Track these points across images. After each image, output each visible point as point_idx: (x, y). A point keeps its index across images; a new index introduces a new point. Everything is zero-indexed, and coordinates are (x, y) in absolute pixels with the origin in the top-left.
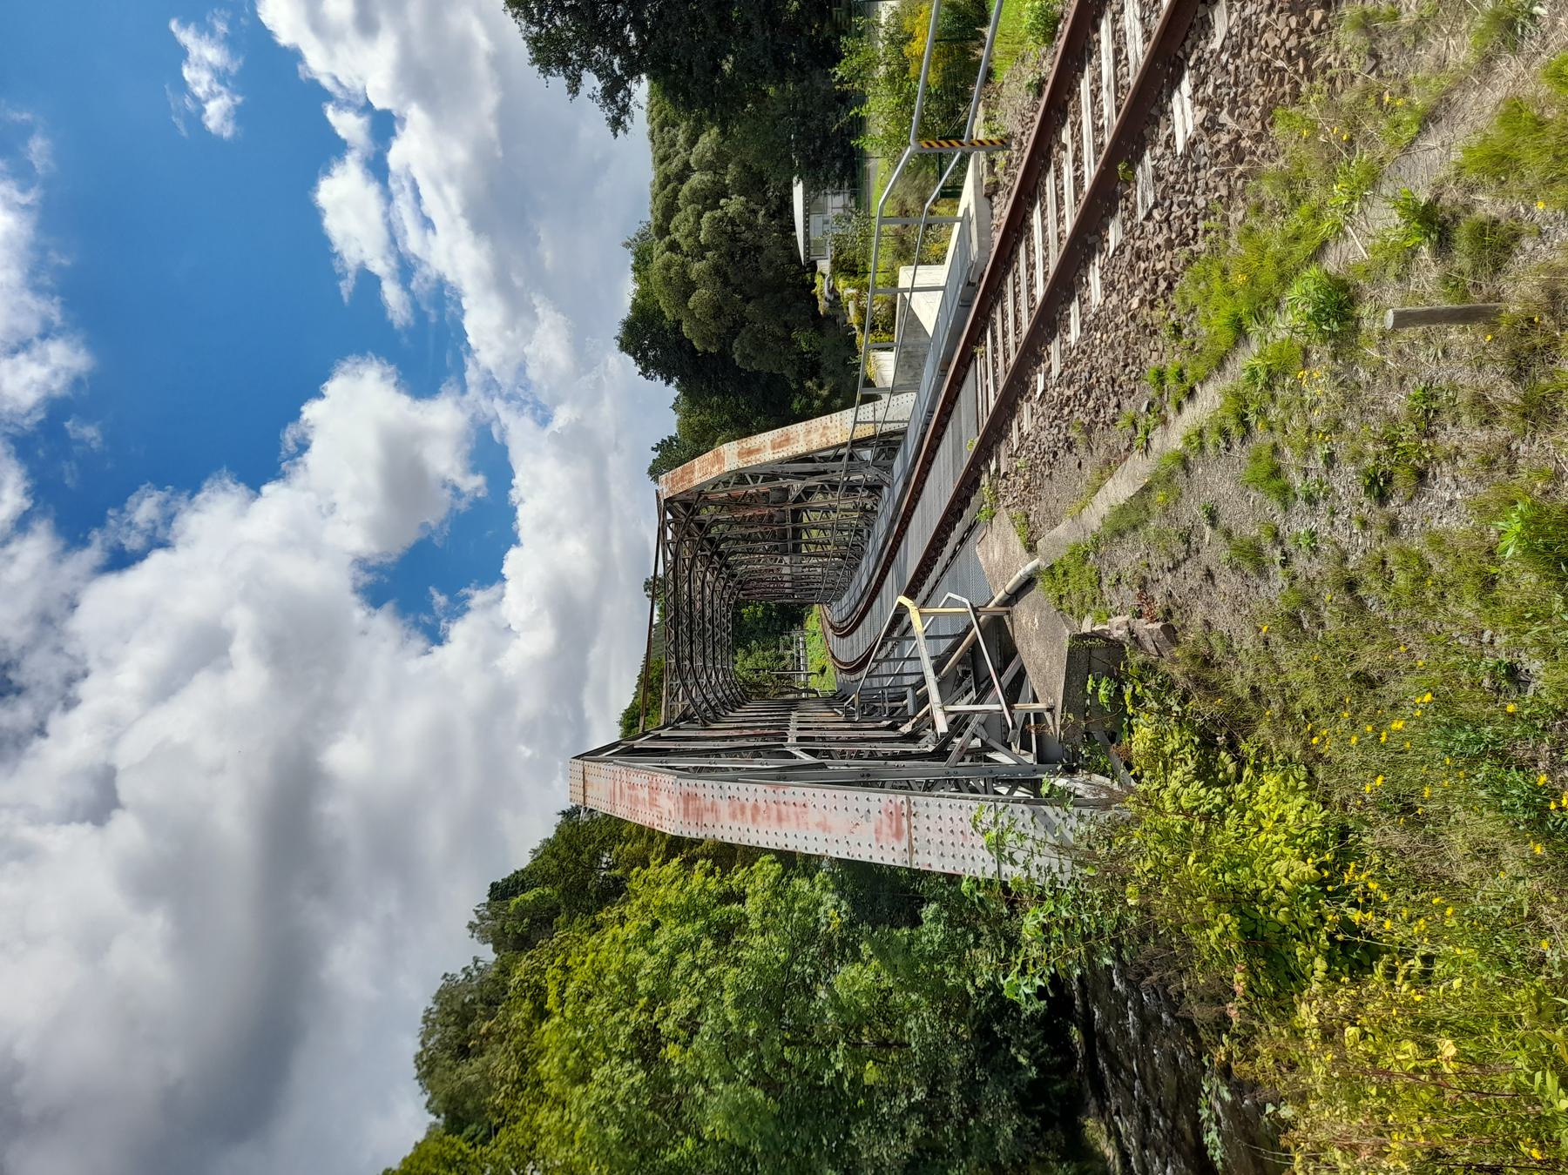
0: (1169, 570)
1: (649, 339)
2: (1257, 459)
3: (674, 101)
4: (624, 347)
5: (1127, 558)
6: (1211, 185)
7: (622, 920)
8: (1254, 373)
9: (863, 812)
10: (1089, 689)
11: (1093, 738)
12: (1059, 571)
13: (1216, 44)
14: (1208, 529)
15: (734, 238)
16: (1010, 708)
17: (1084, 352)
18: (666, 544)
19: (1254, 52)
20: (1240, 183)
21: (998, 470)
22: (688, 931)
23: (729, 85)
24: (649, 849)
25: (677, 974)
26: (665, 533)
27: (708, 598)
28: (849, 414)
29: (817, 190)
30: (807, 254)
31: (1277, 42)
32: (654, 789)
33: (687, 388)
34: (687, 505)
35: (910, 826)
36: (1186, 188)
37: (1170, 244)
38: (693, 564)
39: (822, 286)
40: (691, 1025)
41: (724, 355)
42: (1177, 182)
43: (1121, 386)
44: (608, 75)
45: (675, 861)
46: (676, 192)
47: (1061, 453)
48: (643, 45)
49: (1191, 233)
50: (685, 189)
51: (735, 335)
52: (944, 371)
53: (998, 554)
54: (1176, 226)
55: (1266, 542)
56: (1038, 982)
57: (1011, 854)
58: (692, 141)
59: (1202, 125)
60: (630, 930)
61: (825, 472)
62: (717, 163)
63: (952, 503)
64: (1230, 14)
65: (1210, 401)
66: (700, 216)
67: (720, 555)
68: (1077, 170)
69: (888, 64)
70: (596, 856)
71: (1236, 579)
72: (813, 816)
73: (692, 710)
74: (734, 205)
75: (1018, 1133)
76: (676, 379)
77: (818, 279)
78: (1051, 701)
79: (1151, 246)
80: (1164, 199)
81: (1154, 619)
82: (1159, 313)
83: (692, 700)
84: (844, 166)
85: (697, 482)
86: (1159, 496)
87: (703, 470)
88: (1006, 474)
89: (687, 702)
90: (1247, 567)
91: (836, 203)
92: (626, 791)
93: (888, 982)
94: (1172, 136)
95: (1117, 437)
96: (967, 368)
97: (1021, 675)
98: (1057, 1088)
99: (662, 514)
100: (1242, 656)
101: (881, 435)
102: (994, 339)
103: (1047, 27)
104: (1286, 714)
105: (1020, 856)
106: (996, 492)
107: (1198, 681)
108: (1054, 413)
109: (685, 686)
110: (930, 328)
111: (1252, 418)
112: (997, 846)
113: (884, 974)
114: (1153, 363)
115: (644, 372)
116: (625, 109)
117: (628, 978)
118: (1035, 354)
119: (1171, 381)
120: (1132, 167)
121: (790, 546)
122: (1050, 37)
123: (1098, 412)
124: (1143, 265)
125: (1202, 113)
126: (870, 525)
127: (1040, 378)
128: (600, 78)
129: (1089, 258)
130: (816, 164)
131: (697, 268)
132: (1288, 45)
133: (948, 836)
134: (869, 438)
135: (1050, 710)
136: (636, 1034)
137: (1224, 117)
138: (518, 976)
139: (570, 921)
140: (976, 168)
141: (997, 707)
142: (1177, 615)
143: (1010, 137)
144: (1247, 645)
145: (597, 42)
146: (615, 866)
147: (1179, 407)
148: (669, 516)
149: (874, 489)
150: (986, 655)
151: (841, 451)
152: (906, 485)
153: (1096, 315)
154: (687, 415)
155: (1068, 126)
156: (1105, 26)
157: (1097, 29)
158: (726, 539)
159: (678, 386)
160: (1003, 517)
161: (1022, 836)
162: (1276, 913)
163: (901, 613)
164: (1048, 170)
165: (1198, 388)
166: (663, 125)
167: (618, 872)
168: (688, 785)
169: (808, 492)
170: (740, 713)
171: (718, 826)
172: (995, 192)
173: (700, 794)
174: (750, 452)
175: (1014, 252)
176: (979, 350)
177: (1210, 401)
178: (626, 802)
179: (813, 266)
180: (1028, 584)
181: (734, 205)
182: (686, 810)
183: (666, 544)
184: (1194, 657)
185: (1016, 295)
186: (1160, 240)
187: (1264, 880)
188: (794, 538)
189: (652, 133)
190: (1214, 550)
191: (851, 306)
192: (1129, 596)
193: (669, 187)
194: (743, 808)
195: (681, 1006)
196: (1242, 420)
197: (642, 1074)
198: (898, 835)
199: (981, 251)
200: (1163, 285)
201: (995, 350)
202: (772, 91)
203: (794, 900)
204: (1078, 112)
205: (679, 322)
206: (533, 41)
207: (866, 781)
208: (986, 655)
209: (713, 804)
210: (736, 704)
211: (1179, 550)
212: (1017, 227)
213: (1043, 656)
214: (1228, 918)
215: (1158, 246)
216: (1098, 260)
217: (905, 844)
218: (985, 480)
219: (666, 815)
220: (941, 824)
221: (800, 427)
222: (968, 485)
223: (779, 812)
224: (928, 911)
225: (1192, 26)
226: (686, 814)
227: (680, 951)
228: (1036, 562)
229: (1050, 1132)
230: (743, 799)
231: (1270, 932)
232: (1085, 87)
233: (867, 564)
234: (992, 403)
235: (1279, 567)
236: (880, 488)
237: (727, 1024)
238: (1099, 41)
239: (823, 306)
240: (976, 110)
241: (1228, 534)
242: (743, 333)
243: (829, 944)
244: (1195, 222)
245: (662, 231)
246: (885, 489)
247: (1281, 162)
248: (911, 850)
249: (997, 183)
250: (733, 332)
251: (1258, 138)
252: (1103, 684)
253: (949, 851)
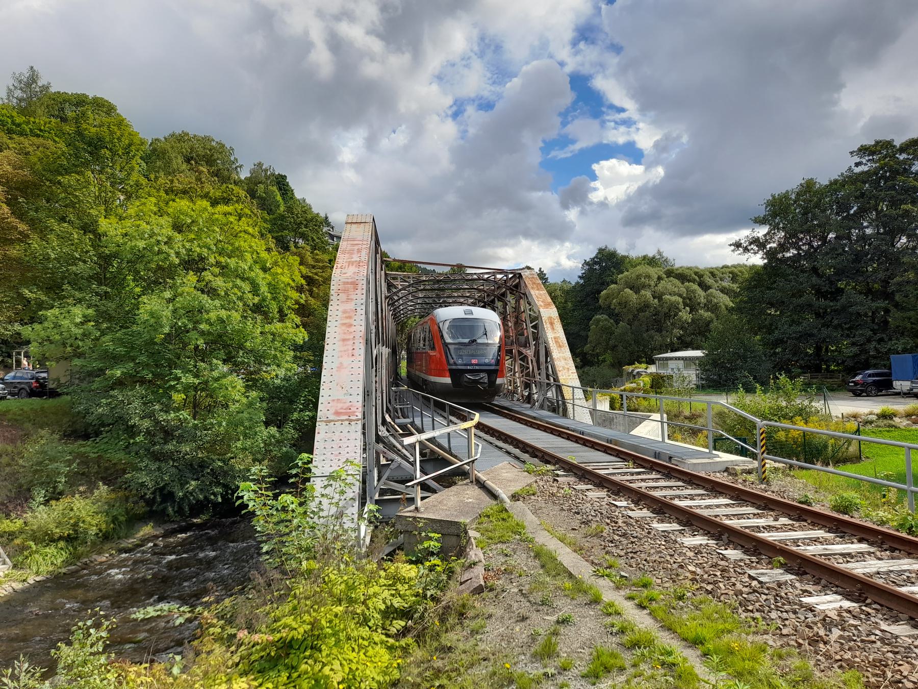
0: (521, 591)
2: (613, 655)
4: (601, 251)
5: (521, 560)
6: (787, 623)
7: (268, 250)
8: (670, 653)
9: (351, 391)
10: (432, 535)
11: (397, 537)
14: (554, 618)
17: (649, 533)
18: (494, 274)
19: (890, 655)
20: (793, 643)
21: (558, 475)
22: (264, 289)
23: (762, 312)
25: (238, 282)
26: (500, 273)
27: (458, 300)
28: (577, 383)
30: (660, 359)
31: (905, 673)
32: (358, 264)
33: (577, 289)
34: (517, 286)
35: (342, 421)
36: (779, 604)
37: (738, 593)
38: (480, 291)
39: (640, 368)
40: (211, 292)
41: (598, 309)
42: (782, 597)
43: (632, 558)
44: (767, 240)
45: (303, 282)
46: (694, 281)
47: (579, 517)
48: (784, 260)
49: (750, 608)
50: (695, 287)
51: (609, 315)
52: (610, 441)
53: (506, 475)
54: (752, 597)
56: (251, 504)
57: (331, 485)
58: (723, 290)
59: (826, 616)
61: (539, 369)
62: (712, 307)
63: (523, 443)
64: (909, 637)
65: (642, 621)
66: (680, 296)
68: (763, 527)
70: (303, 236)
71: (524, 637)
72: (346, 361)
73: (394, 290)
74: (685, 315)
75: (142, 485)
76: (582, 281)
77: (644, 365)
78: (422, 509)
79: (733, 580)
80: (768, 589)
81: (485, 578)
83: (400, 290)
84: (714, 381)
85: (532, 292)
86: (568, 584)
88: (557, 481)
89: (400, 287)
90: (536, 648)
91: (692, 375)
92: (356, 248)
93: (233, 408)
94: (810, 594)
96: (617, 456)
97: (434, 491)
98: (170, 509)
99: (512, 272)
100: (472, 641)
101: (564, 404)
102: (639, 473)
103: (845, 508)
104: (438, 673)
105: (328, 491)
106: (543, 474)
107: (447, 608)
108: (604, 512)
109: (409, 286)
110: (634, 432)
111: (638, 652)
113: (237, 405)
115: (586, 263)
116: (746, 250)
117: (237, 253)
118: (639, 500)
119: (645, 592)
120: (782, 566)
122: (837, 508)
123: (612, 542)
124: (718, 573)
125: (833, 615)
127: (624, 504)
128: (765, 236)
129: (712, 536)
132: (905, 681)
133: (338, 448)
135: (416, 508)
136: (202, 259)
137: (836, 632)
138: (236, 189)
139: (265, 221)
140: (744, 462)
141: (418, 476)
142: (491, 595)
143: (768, 483)
144: (482, 646)
145: (786, 233)
146: (296, 247)
147: (631, 598)
148: (510, 276)
150: (443, 469)
151: (552, 379)
152: (534, 418)
153: (676, 542)
154: (562, 289)
156: (864, 547)
159: (577, 283)
160: (531, 479)
161: (342, 492)
162: (306, 663)
165: (645, 612)
166: (734, 273)
169: (524, 358)
170: (390, 318)
171: (338, 302)
172: (730, 474)
173: (357, 292)
174: (552, 324)
175: (698, 486)
177: (642, 621)
178: (349, 248)
179: (651, 362)
180: (494, 496)
181: (685, 315)
182: (347, 283)
183: (494, 274)
184: (464, 606)
185: (671, 487)
186: (739, 586)
187: (328, 656)
189: (727, 267)
190: (543, 622)
191: (634, 385)
192: (498, 562)
193: (696, 278)
194: (350, 317)
195: (219, 282)
196: (635, 645)
197: (177, 261)
198: (337, 413)
199: (692, 465)
200: (709, 587)
201: (632, 474)
203: (281, 352)
204: (801, 528)
206: (786, 196)
208: (443, 469)
210: (395, 316)
211: (537, 597)
212: (715, 488)
213: (450, 504)
214: (301, 630)
215: (734, 585)
216: (712, 542)
217: (331, 417)
218: (550, 467)
219: (344, 271)
220: (344, 440)
221: (568, 354)
222: (545, 457)
223: (348, 340)
224: (273, 430)
225: (891, 609)
226: (345, 283)
227: (251, 284)
228: (508, 500)
229: (144, 504)
230: (355, 317)
231: (292, 660)
232: (820, 533)
234: (602, 472)
235: (542, 671)
236: (529, 402)
237: (208, 312)
238: (852, 543)
239: (630, 368)
240: (779, 462)
241: (555, 633)
242: (615, 318)
243: (255, 372)
244: (757, 611)
245: (670, 273)
246: (529, 406)
247: (818, 674)
248: (328, 422)
249: (736, 475)
251: (828, 656)
252: (436, 544)
253: (329, 445)
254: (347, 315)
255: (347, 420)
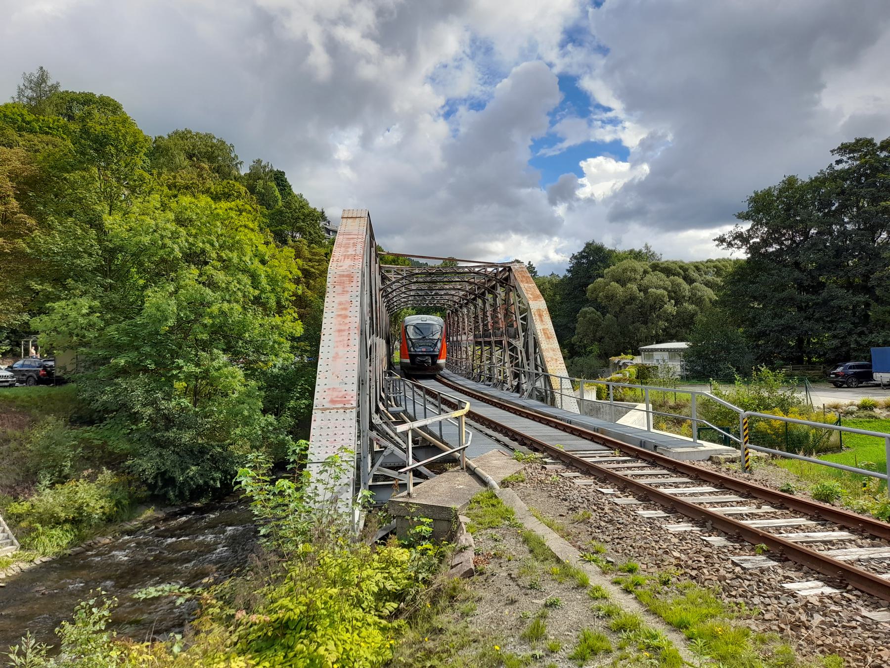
0: (510, 575)
1: (592, 260)
2: (600, 638)
3: (733, 274)
4: (588, 245)
5: (510, 545)
6: (769, 608)
7: (267, 243)
8: (655, 637)
9: (346, 380)
10: (424, 520)
11: (390, 522)
12: (494, 501)
13: (865, 612)
14: (542, 602)
15: (653, 308)
16: (410, 470)
17: (635, 519)
21: (546, 463)
22: (264, 281)
24: (304, 259)
26: (491, 267)
28: (565, 373)
29: (684, 357)
30: (645, 350)
32: (354, 257)
33: (565, 282)
34: (507, 279)
35: (337, 409)
36: (762, 590)
37: (722, 579)
38: (471, 283)
39: (625, 359)
40: (212, 284)
41: (586, 302)
42: (764, 583)
43: (618, 543)
45: (300, 274)
46: (678, 275)
47: (566, 503)
48: (767, 255)
49: (734, 593)
52: (597, 430)
53: (496, 462)
55: (546, 645)
59: (808, 602)
60: (262, 248)
61: (528, 359)
62: (698, 301)
65: (628, 606)
66: (665, 289)
67: (474, 299)
68: (746, 515)
69: (769, 398)
70: (300, 230)
71: (513, 620)
72: (342, 351)
73: (388, 283)
74: (670, 308)
76: (569, 275)
78: (414, 495)
79: (717, 566)
80: (751, 574)
82: (673, 569)
83: (394, 283)
85: (522, 285)
86: (556, 568)
87: (529, 291)
89: (394, 280)
91: (677, 366)
92: (352, 241)
94: (792, 580)
95: (585, 540)
96: (603, 444)
99: (502, 265)
102: (625, 462)
105: (324, 476)
106: (532, 462)
107: (438, 590)
108: (591, 499)
109: (403, 278)
112: (328, 463)
114: (639, 565)
115: (574, 257)
116: (730, 245)
119: (631, 577)
120: (764, 552)
121: (479, 340)
124: (702, 559)
125: (815, 601)
126: (495, 386)
127: (611, 491)
128: (748, 231)
130: (699, 356)
131: (634, 287)
133: (333, 435)
134: (551, 386)
137: (818, 618)
139: (264, 216)
140: (727, 451)
141: (411, 463)
142: (481, 578)
143: (751, 472)
147: (617, 583)
148: (500, 269)
149: (518, 389)
150: (435, 456)
152: (523, 407)
153: (660, 528)
155: (773, 510)
157: (841, 529)
158: (484, 303)
159: (565, 276)
160: (520, 466)
161: (338, 478)
162: (302, 643)
163: (455, 407)
164: (740, 496)
165: (631, 596)
166: (717, 267)
167: (290, 242)
168: (358, 277)
169: (514, 349)
172: (714, 463)
173: (352, 284)
174: (540, 316)
175: (683, 474)
176: (617, 452)
177: (628, 606)
178: (345, 242)
179: (637, 353)
180: (484, 482)
182: (343, 276)
184: (454, 589)
186: (722, 572)
187: (323, 636)
188: (485, 342)
190: (531, 605)
192: (488, 547)
194: (346, 309)
195: (220, 277)
196: (621, 628)
198: (332, 401)
199: (676, 454)
200: (694, 573)
201: (618, 462)
202: (741, 330)
204: (784, 516)
205: (602, 277)
206: (768, 193)
207: (361, 383)
208: (435, 456)
209: (347, 291)
210: (389, 308)
211: (526, 581)
212: (700, 477)
213: (441, 490)
214: (297, 611)
215: (718, 570)
219: (340, 264)
220: (340, 427)
221: (556, 344)
222: (534, 446)
223: (344, 330)
224: (271, 418)
225: (871, 596)
226: (341, 276)
228: (497, 487)
229: (146, 488)
230: (351, 309)
231: (288, 640)
232: (802, 521)
233: (470, 384)
235: (530, 653)
236: (518, 392)
237: (209, 305)
238: (834, 531)
239: (615, 359)
240: (762, 451)
241: (543, 616)
242: (604, 312)
244: (740, 596)
245: (655, 267)
246: (518, 395)
248: (324, 410)
250: (599, 307)
251: (809, 641)
254: (342, 306)
255: (342, 408)
